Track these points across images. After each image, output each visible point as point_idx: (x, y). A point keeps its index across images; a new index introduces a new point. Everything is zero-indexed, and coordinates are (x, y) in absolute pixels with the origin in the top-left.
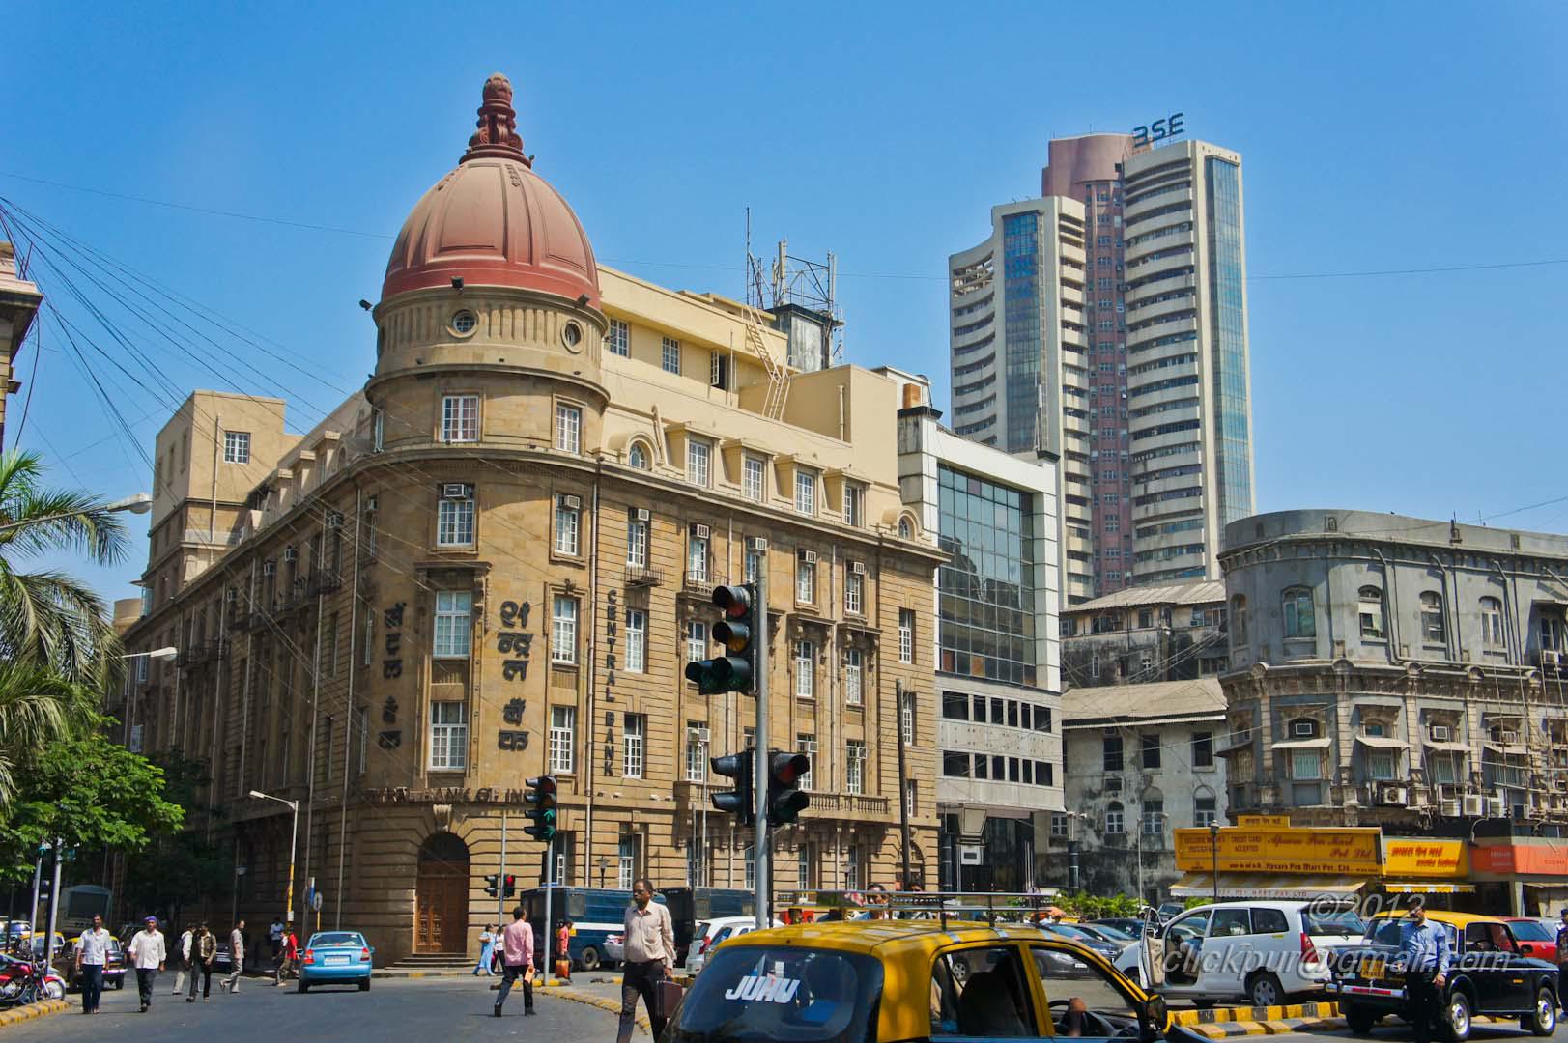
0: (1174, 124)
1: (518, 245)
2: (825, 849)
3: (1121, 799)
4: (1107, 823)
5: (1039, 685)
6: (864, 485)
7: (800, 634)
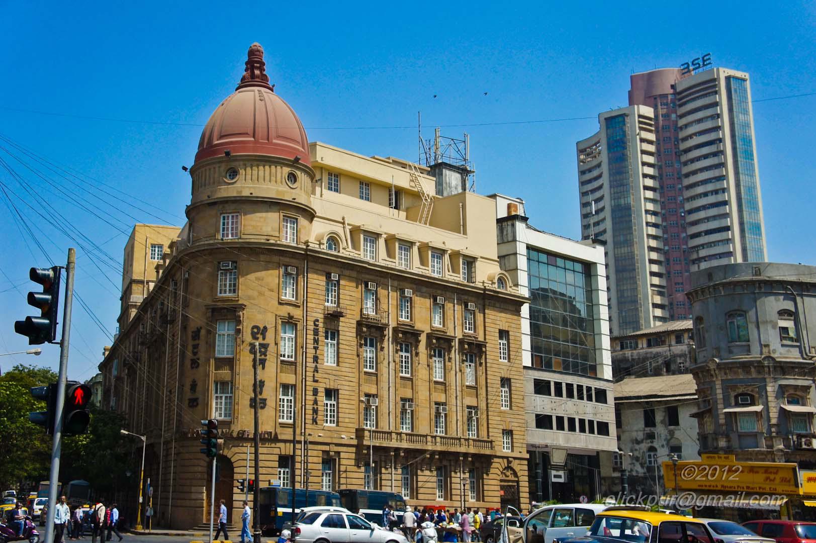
1: (261, 132)
3: (655, 445)
5: (599, 376)
7: (466, 349)
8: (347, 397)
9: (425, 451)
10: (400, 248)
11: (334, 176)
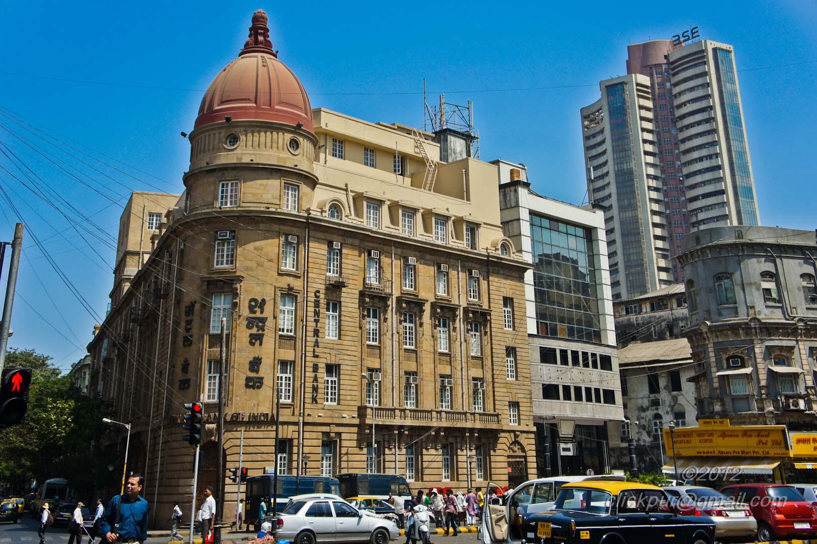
0: (694, 32)
1: (263, 98)
2: (459, 446)
3: (660, 412)
4: (654, 428)
5: (603, 343)
6: (478, 225)
7: (470, 318)
8: (349, 372)
9: (428, 428)
10: (404, 215)
11: (339, 143)
